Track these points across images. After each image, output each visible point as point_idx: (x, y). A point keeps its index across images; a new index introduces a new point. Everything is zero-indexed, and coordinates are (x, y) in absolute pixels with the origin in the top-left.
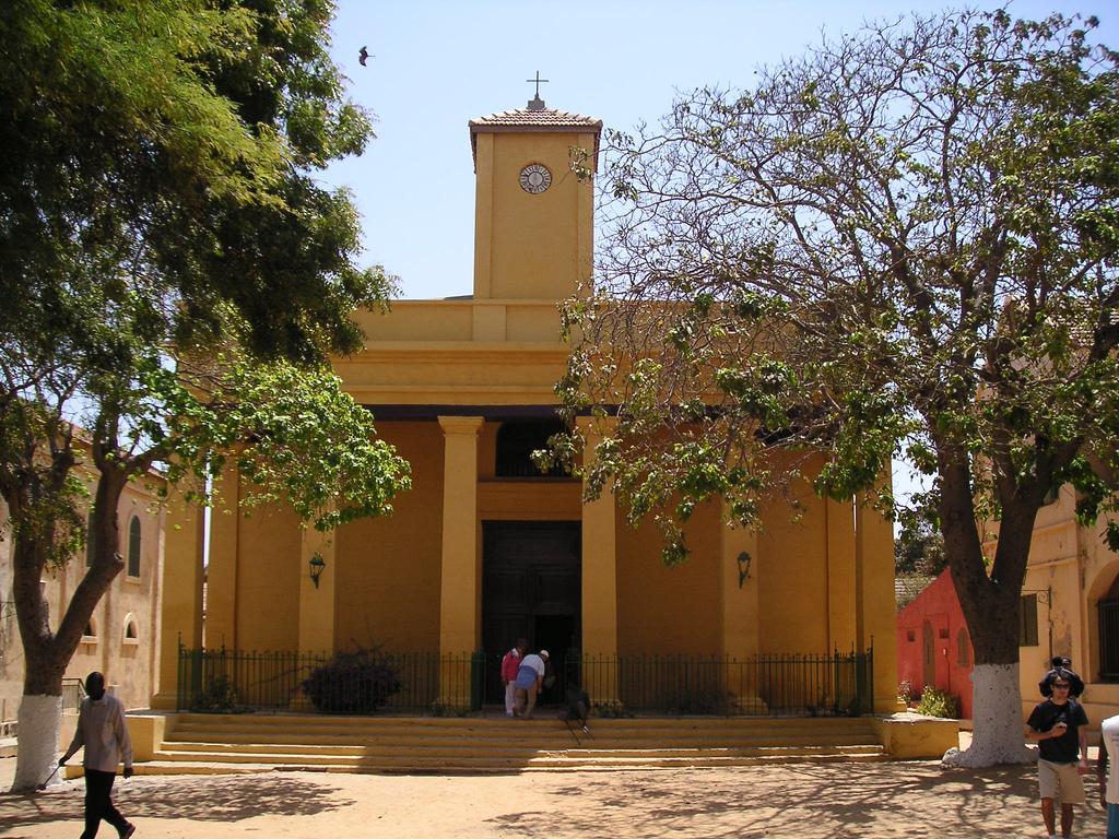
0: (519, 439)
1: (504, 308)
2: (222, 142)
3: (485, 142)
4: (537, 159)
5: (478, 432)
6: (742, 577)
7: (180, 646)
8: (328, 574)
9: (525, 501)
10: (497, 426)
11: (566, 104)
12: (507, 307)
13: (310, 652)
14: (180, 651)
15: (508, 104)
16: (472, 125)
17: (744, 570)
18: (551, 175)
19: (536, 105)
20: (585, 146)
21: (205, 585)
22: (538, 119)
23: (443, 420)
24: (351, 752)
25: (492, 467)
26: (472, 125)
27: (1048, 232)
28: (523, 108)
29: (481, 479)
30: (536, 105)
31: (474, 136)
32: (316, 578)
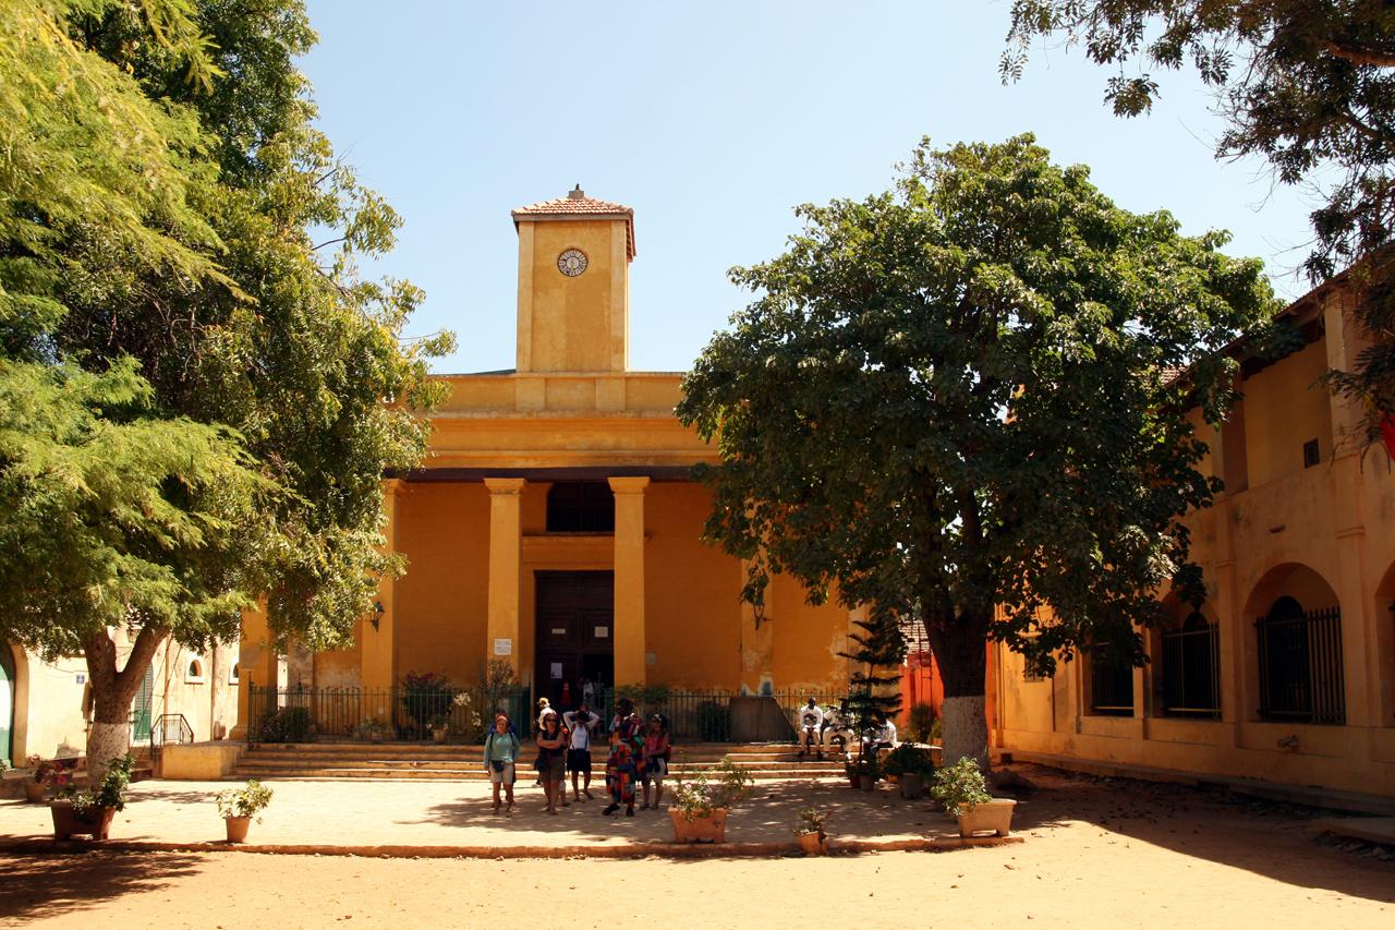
0: (574, 502)
1: (543, 381)
2: (1235, 478)
3: (528, 230)
4: (575, 245)
5: (521, 492)
6: (758, 620)
7: (251, 683)
8: (387, 621)
9: (573, 552)
10: (545, 488)
11: (603, 194)
12: (546, 379)
13: (378, 688)
14: (251, 688)
15: (551, 196)
16: (514, 214)
17: (758, 615)
18: (587, 259)
19: (576, 194)
20: (619, 231)
21: (1137, 673)
22: (577, 208)
23: (489, 482)
24: (360, 774)
25: (541, 521)
26: (514, 214)
27: (913, 289)
28: (564, 199)
29: (526, 533)
30: (576, 194)
31: (517, 224)
32: (375, 623)
